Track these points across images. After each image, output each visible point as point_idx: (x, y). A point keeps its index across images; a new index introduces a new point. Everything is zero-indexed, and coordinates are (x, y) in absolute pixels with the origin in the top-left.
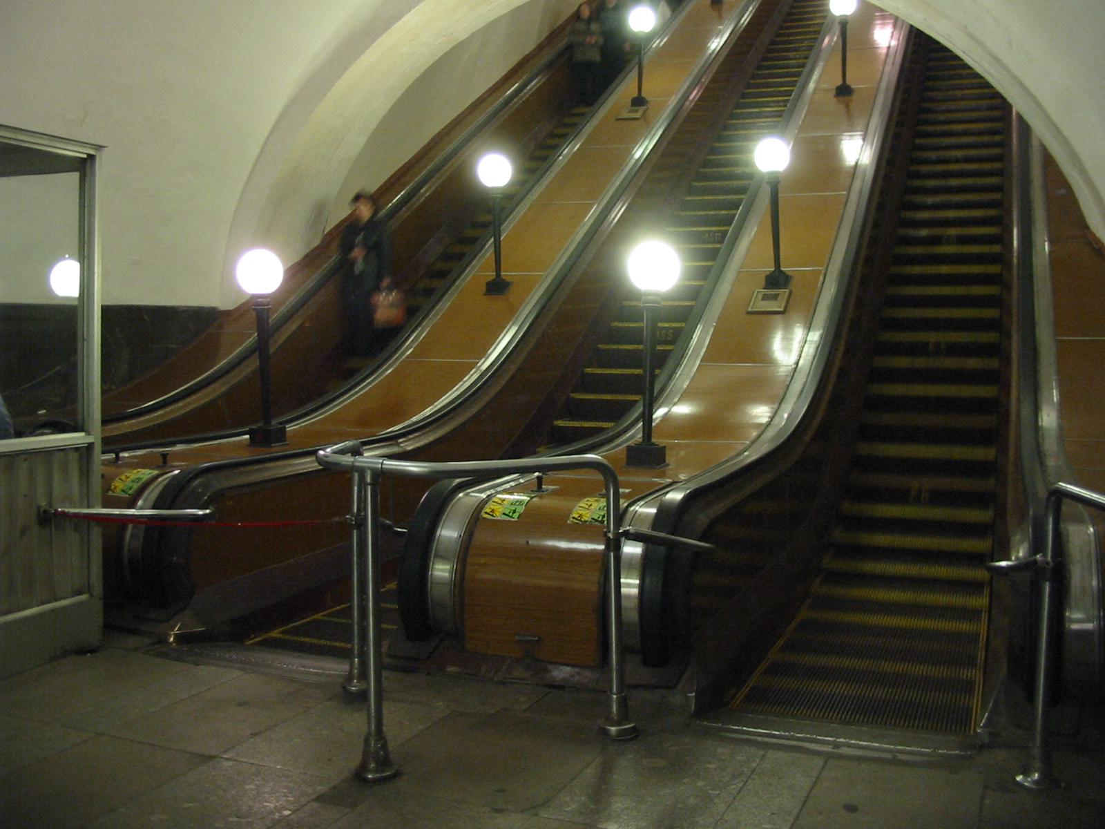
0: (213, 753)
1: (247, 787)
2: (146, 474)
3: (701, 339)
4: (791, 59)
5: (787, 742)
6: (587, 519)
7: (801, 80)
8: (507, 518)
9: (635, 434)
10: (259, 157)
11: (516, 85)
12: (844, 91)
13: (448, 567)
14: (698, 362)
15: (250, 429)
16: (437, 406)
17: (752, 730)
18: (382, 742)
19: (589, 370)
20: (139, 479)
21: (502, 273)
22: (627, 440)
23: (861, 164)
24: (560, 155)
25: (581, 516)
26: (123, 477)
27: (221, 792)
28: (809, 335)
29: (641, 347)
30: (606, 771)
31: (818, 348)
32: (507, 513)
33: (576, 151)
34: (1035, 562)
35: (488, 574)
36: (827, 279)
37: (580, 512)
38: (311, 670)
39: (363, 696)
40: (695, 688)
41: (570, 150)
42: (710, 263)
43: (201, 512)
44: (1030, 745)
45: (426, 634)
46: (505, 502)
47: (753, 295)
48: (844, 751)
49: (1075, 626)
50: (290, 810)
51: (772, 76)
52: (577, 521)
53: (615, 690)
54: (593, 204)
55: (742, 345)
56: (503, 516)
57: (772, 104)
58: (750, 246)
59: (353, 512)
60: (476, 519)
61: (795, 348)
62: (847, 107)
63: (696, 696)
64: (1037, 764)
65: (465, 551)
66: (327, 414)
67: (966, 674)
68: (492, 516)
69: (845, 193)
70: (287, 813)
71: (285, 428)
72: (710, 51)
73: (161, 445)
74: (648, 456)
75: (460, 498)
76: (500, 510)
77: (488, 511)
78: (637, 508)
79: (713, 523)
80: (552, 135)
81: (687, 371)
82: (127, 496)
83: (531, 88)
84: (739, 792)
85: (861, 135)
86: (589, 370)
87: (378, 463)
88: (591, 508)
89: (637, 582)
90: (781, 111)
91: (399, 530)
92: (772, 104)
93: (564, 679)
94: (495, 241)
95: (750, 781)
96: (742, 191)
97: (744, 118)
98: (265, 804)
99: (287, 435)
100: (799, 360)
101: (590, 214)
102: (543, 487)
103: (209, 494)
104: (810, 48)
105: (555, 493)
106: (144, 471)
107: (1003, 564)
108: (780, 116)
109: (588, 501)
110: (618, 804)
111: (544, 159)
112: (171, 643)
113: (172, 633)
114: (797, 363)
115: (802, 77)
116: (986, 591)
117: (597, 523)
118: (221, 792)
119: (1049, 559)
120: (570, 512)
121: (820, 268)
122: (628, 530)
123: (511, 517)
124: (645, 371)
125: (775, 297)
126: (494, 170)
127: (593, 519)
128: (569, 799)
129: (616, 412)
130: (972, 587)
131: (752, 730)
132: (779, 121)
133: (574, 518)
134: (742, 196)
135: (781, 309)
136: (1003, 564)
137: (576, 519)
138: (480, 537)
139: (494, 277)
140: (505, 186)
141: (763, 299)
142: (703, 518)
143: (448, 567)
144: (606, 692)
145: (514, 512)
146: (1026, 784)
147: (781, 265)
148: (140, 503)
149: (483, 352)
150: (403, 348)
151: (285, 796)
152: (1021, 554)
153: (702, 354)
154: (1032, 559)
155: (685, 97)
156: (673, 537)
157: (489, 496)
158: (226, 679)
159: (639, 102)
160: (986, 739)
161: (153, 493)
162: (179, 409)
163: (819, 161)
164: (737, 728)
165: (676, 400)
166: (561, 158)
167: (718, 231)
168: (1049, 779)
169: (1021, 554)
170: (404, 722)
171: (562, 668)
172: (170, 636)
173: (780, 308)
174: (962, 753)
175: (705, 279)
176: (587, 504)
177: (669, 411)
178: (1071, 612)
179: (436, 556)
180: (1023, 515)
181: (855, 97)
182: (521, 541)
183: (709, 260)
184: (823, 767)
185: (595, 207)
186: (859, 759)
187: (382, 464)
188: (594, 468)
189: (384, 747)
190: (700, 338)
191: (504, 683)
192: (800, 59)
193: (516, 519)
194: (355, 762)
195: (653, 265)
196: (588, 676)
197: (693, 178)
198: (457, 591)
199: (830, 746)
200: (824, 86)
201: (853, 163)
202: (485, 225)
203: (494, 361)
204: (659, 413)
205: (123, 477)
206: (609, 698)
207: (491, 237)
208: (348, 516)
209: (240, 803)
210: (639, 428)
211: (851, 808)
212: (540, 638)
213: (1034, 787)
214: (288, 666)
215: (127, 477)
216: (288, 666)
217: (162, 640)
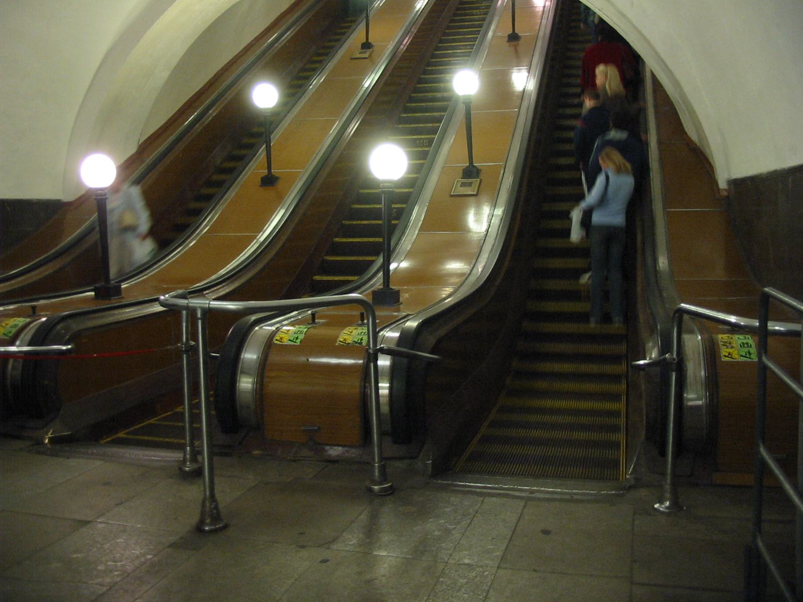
0: (90, 519)
1: (118, 541)
2: (21, 321)
3: (419, 215)
4: (475, 15)
5: (498, 491)
6: (349, 342)
7: (483, 30)
8: (293, 343)
9: (377, 282)
10: (90, 87)
11: (276, 35)
12: (514, 37)
13: (251, 380)
14: (417, 232)
15: (95, 287)
16: (229, 268)
17: (472, 484)
18: (214, 503)
19: (337, 239)
20: (16, 326)
21: (272, 171)
22: (372, 286)
23: (527, 90)
24: (310, 85)
25: (345, 340)
26: (3, 324)
27: (99, 546)
28: (495, 210)
29: (380, 222)
30: (374, 517)
31: (501, 219)
32: (292, 339)
33: (322, 82)
34: (665, 359)
35: (276, 386)
36: (506, 170)
37: (345, 337)
38: (153, 458)
39: (198, 473)
40: (431, 457)
41: (317, 81)
42: (421, 162)
43: (64, 348)
44: (663, 483)
45: (238, 428)
46: (290, 332)
47: (454, 183)
48: (537, 495)
49: (690, 403)
50: (151, 555)
51: (461, 27)
52: (343, 344)
53: (376, 459)
54: (337, 120)
55: (447, 220)
56: (289, 342)
57: (462, 48)
58: (450, 149)
59: (182, 341)
60: (269, 345)
61: (483, 221)
62: (516, 51)
63: (432, 463)
64: (668, 495)
65: (263, 368)
66: (150, 275)
67: (614, 437)
68: (281, 341)
69: (517, 110)
70: (149, 557)
71: (121, 286)
72: (417, 9)
73: (31, 301)
74: (388, 296)
75: (256, 330)
76: (286, 338)
77: (278, 338)
78: (385, 333)
79: (439, 341)
80: (303, 70)
81: (410, 238)
82: (8, 338)
83: (287, 37)
84: (469, 526)
85: (527, 69)
86: (337, 239)
87: (206, 303)
88: (352, 334)
89: (388, 385)
90: (469, 52)
91: (214, 354)
92: (462, 48)
93: (338, 456)
94: (266, 146)
95: (475, 519)
96: (444, 109)
97: (450, 57)
98: (133, 552)
99: (123, 291)
100: (489, 228)
101: (334, 128)
102: (316, 320)
103: (69, 334)
104: (488, 7)
105: (324, 325)
106: (19, 319)
107: (642, 362)
108: (469, 56)
109: (349, 329)
110: (385, 538)
111: (300, 86)
112: (46, 444)
113: (47, 436)
114: (487, 231)
115: (483, 28)
116: (624, 382)
117: (357, 344)
118: (99, 546)
119: (675, 356)
120: (338, 337)
121: (501, 164)
122: (383, 347)
123: (295, 342)
124: (384, 240)
125: (470, 184)
126: (265, 95)
127: (354, 341)
128: (350, 537)
129: (360, 269)
130: (616, 378)
131: (472, 484)
132: (467, 60)
133: (340, 341)
134: (442, 114)
135: (475, 193)
136: (642, 362)
137: (342, 342)
138: (274, 358)
139: (267, 174)
140: (273, 107)
141: (461, 186)
142: (431, 339)
143: (251, 380)
144: (370, 464)
145: (297, 338)
146: (661, 509)
147: (474, 161)
148: (18, 343)
149: (260, 229)
150: (202, 226)
151: (146, 545)
152: (653, 356)
153: (419, 225)
154: (662, 357)
155: (400, 42)
156: (412, 352)
157: (277, 328)
158: (88, 467)
159: (367, 46)
160: (633, 482)
161: (28, 335)
162: (34, 276)
163: (498, 85)
164: (462, 484)
165: (402, 259)
166: (311, 87)
167: (426, 139)
168: (675, 504)
169: (653, 356)
170: (233, 488)
171: (335, 448)
172: (46, 438)
173: (474, 192)
174: (617, 493)
175: (420, 173)
176: (349, 331)
177: (398, 266)
178: (687, 393)
179: (242, 372)
180: (652, 330)
181: (521, 42)
182: (303, 359)
183: (420, 159)
184: (525, 507)
185: (338, 122)
186: (548, 500)
187: (209, 304)
188: (362, 305)
189: (216, 508)
190: (418, 214)
191: (295, 461)
192: (480, 15)
193: (298, 344)
194: (194, 520)
195: (387, 161)
196: (354, 453)
197: (408, 100)
198: (258, 396)
199: (528, 493)
200: (499, 34)
201: (521, 89)
202: (259, 135)
203: (266, 238)
204: (393, 266)
205: (3, 324)
206: (373, 466)
207: (263, 144)
208: (179, 345)
209: (115, 552)
210: (380, 276)
211: (546, 532)
212: (319, 428)
213: (667, 511)
214: (135, 456)
215: (7, 324)
216: (135, 456)
217: (40, 442)
